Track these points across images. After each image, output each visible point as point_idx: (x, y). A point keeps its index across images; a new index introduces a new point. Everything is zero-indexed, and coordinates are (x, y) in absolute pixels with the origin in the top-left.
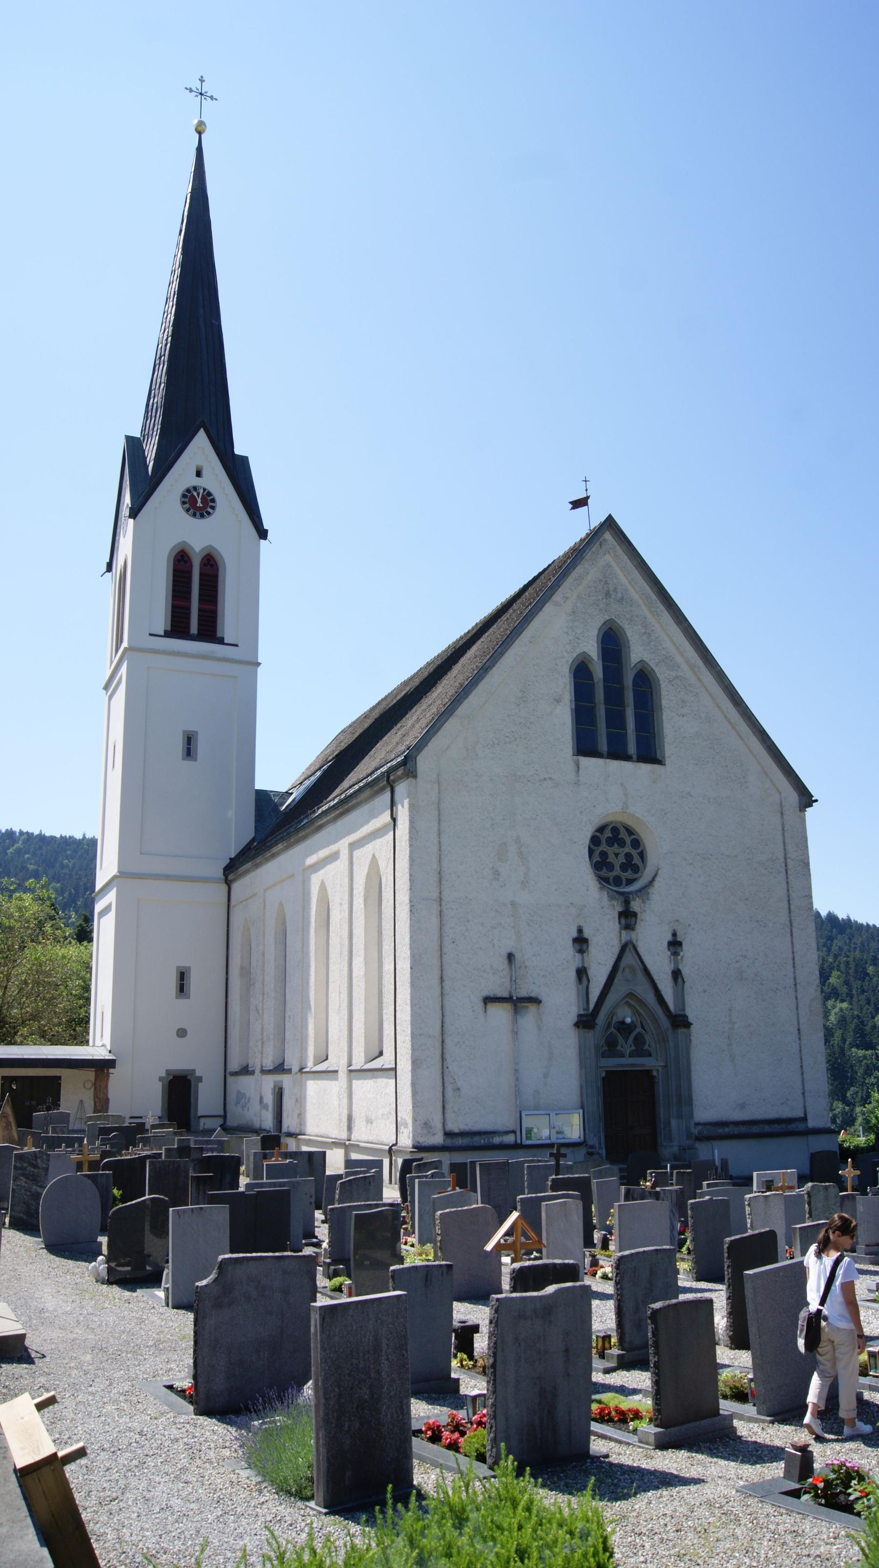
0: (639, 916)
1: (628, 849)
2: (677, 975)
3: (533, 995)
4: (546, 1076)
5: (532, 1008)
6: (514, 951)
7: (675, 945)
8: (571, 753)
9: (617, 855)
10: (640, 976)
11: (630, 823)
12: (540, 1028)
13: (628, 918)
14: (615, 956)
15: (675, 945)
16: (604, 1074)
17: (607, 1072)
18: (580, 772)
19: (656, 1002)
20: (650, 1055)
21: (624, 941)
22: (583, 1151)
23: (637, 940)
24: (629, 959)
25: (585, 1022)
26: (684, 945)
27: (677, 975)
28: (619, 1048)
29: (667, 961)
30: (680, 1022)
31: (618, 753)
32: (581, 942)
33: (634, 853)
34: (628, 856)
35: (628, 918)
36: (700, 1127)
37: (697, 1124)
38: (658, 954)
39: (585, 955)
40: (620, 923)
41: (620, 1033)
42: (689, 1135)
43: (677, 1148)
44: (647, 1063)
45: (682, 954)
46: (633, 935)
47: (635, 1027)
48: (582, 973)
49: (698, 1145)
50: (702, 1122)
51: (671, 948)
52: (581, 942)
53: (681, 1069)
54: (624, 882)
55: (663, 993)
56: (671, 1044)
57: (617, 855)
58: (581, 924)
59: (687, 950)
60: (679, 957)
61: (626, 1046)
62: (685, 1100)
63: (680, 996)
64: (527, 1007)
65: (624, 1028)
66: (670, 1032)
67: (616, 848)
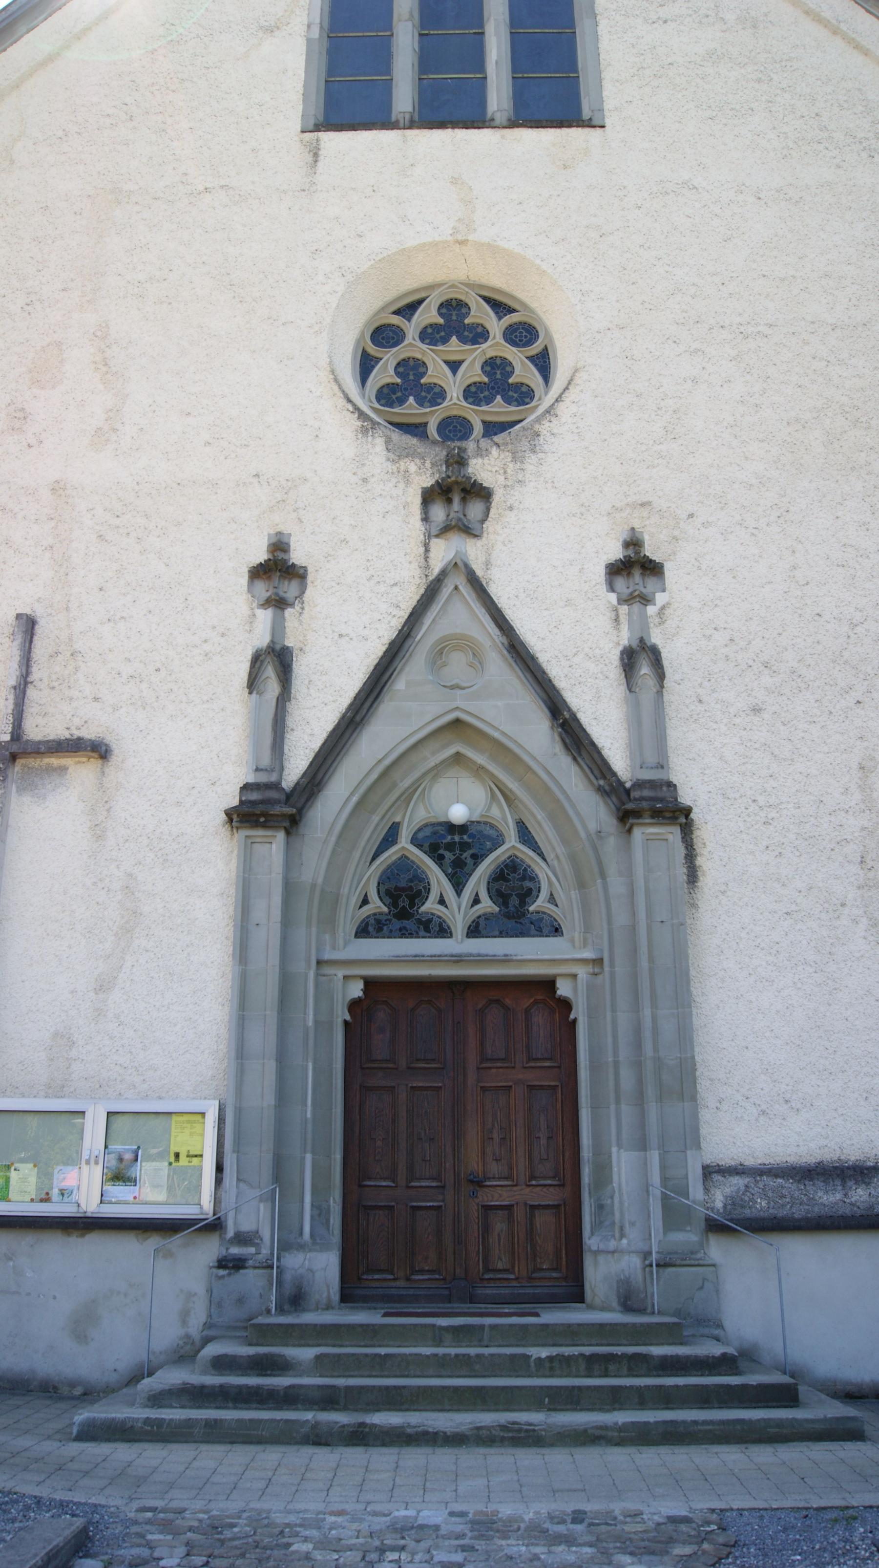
0: (496, 499)
1: (496, 345)
2: (640, 660)
3: (89, 733)
4: (103, 986)
5: (81, 772)
6: (39, 612)
7: (635, 568)
8: (296, 124)
9: (454, 366)
10: (499, 668)
11: (496, 279)
12: (98, 833)
13: (456, 498)
14: (403, 614)
15: (635, 568)
16: (356, 990)
17: (370, 984)
18: (320, 164)
19: (558, 748)
20: (557, 931)
21: (436, 568)
22: (209, 1250)
23: (488, 564)
24: (458, 616)
25: (267, 810)
26: (670, 572)
27: (640, 660)
28: (430, 906)
29: (603, 621)
30: (650, 805)
31: (451, 106)
32: (278, 573)
33: (516, 356)
34: (496, 368)
35: (456, 498)
36: (737, 1182)
37: (709, 1172)
38: (568, 602)
39: (288, 612)
40: (426, 519)
41: (439, 860)
42: (675, 1214)
43: (636, 1261)
44: (523, 955)
45: (661, 598)
46: (474, 552)
47: (498, 841)
48: (275, 663)
49: (717, 1249)
50: (750, 1162)
51: (620, 583)
52: (278, 573)
53: (665, 979)
54: (372, 350)
55: (586, 719)
56: (617, 884)
57: (454, 366)
58: (284, 528)
59: (681, 587)
60: (651, 610)
61: (456, 903)
62: (675, 1080)
63: (650, 728)
64: (63, 769)
65: (456, 846)
66: (611, 844)
67: (473, 371)
